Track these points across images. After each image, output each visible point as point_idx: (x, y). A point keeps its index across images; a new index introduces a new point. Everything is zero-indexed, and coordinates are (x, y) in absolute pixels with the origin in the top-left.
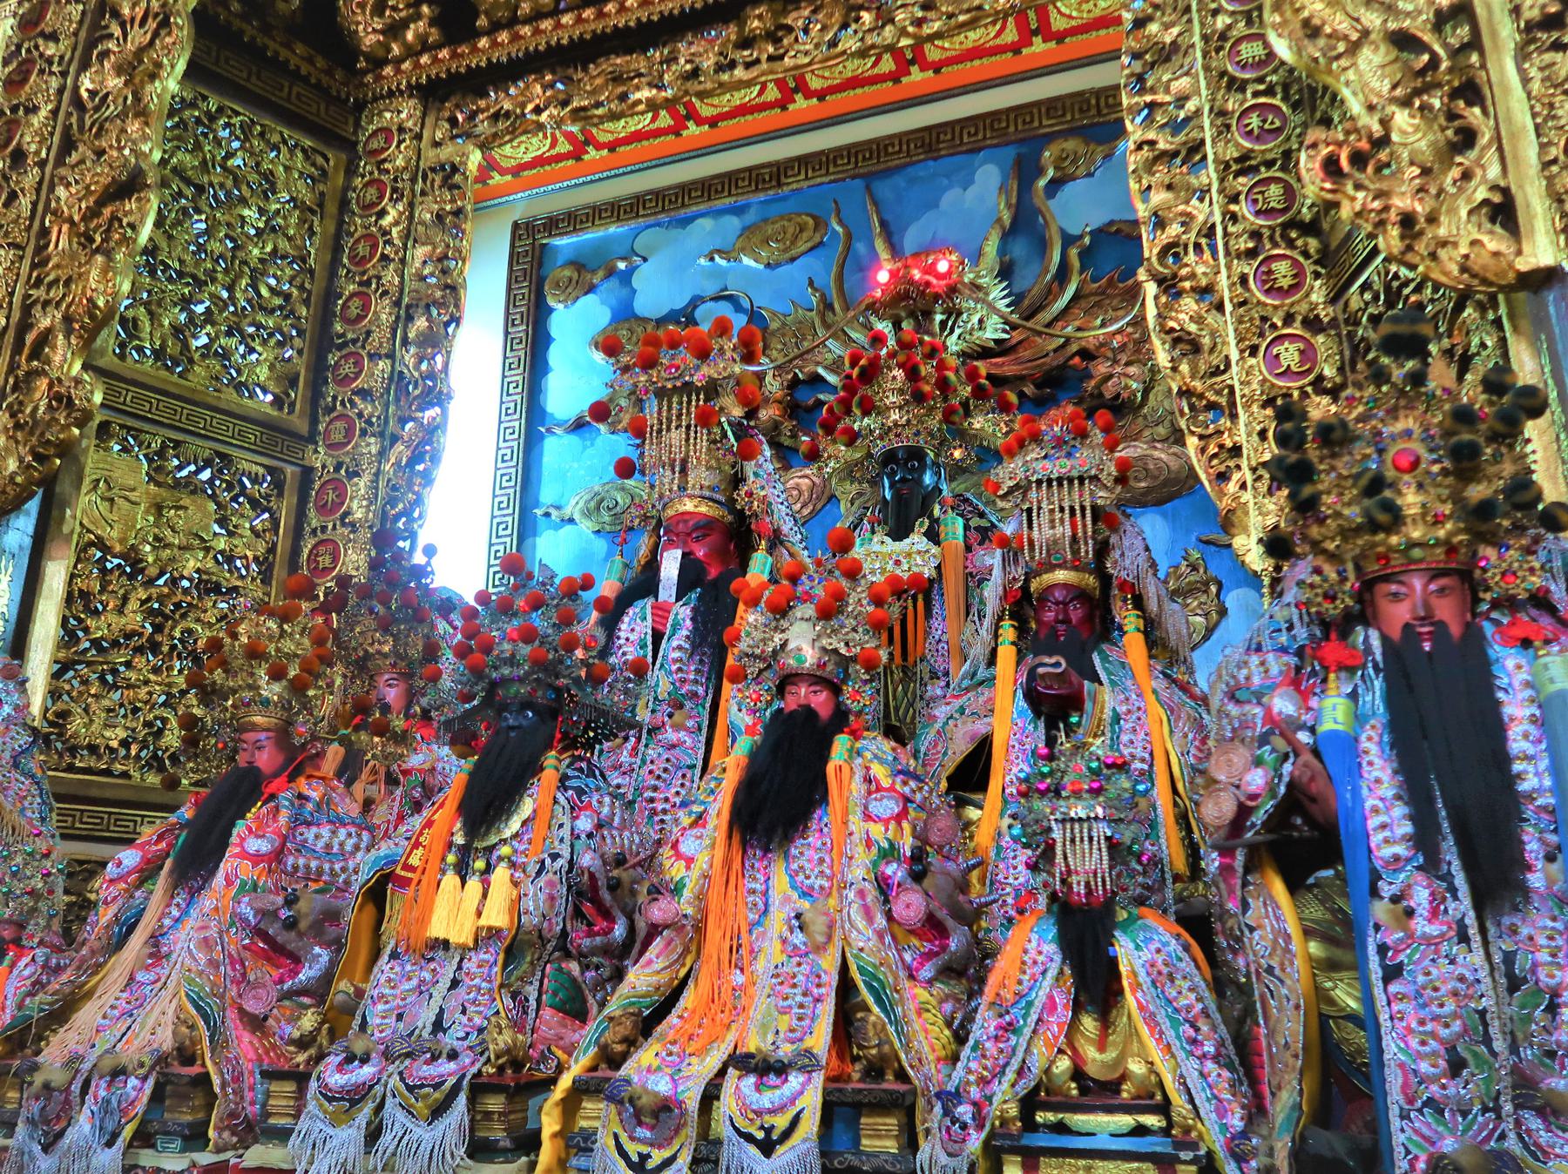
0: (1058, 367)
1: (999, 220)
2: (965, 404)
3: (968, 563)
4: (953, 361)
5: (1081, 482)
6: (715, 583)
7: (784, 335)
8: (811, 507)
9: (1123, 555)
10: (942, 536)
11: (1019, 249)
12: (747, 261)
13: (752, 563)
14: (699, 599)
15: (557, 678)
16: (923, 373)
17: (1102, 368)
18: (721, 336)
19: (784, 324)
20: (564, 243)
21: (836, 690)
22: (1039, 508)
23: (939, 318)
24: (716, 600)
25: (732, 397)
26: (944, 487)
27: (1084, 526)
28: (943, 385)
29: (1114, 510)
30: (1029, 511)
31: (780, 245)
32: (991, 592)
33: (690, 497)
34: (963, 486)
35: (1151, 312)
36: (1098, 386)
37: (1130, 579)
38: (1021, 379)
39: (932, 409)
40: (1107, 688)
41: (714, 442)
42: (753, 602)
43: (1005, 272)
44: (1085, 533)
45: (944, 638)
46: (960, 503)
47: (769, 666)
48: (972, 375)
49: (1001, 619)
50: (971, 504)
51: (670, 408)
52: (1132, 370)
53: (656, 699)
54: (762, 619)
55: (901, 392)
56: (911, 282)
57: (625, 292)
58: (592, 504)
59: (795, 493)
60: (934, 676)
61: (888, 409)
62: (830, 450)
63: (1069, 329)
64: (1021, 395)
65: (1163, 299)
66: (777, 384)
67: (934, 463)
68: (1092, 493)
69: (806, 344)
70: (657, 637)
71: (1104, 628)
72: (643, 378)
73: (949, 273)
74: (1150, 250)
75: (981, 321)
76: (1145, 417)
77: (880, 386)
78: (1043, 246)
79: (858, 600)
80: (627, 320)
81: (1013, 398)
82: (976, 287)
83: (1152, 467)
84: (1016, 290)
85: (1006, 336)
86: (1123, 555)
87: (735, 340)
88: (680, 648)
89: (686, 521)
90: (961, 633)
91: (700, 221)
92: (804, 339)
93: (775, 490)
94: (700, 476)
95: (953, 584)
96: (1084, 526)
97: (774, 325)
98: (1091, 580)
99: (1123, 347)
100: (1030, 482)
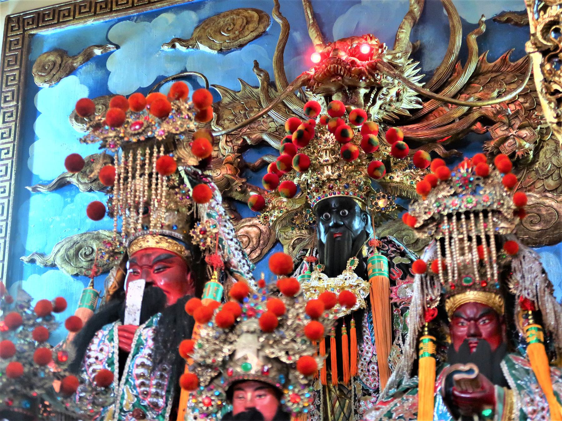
0: (463, 131)
1: (411, 12)
2: (387, 162)
3: (393, 295)
4: (375, 127)
5: (486, 217)
6: (174, 308)
7: (234, 108)
8: (258, 252)
9: (523, 277)
10: (370, 272)
11: (428, 36)
12: (203, 48)
13: (205, 290)
14: (160, 322)
15: (32, 388)
16: (351, 136)
17: (499, 132)
18: (178, 99)
19: (234, 98)
20: (49, 34)
21: (278, 394)
22: (451, 238)
23: (363, 91)
24: (175, 321)
25: (189, 149)
26: (371, 231)
27: (490, 252)
28: (368, 145)
29: (514, 238)
30: (442, 240)
31: (231, 35)
32: (412, 319)
33: (153, 234)
34: (387, 232)
35: (538, 78)
36: (497, 147)
37: (530, 297)
38: (433, 141)
39: (359, 165)
40: (514, 391)
41: (173, 187)
42: (206, 319)
43: (417, 54)
44: (490, 258)
45: (374, 360)
46: (385, 244)
47: (220, 374)
48: (392, 138)
49: (421, 334)
50: (394, 245)
51: (135, 160)
52: (524, 133)
53: (121, 410)
54: (212, 333)
55: (333, 152)
56: (339, 61)
57: (100, 74)
58: (72, 252)
59: (245, 239)
60: (366, 393)
61: (322, 166)
62: (274, 201)
63: (472, 99)
64: (434, 155)
65: (548, 67)
66: (229, 149)
67: (362, 211)
68: (495, 225)
69: (252, 115)
70: (123, 355)
71: (511, 342)
72: (112, 134)
73: (371, 55)
74: (536, 27)
75: (398, 94)
76: (537, 171)
77: (315, 148)
78: (447, 33)
79: (297, 316)
80: (102, 97)
81: (426, 155)
82: (392, 66)
83: (544, 213)
84: (426, 69)
85: (419, 107)
86: (523, 277)
87: (190, 102)
88: (143, 365)
89: (149, 256)
90: (388, 354)
91: (163, 15)
92: (252, 111)
93: (226, 234)
94: (161, 216)
95: (380, 313)
96: (490, 252)
97: (226, 100)
98: (497, 300)
99: (516, 114)
100: (442, 216)
